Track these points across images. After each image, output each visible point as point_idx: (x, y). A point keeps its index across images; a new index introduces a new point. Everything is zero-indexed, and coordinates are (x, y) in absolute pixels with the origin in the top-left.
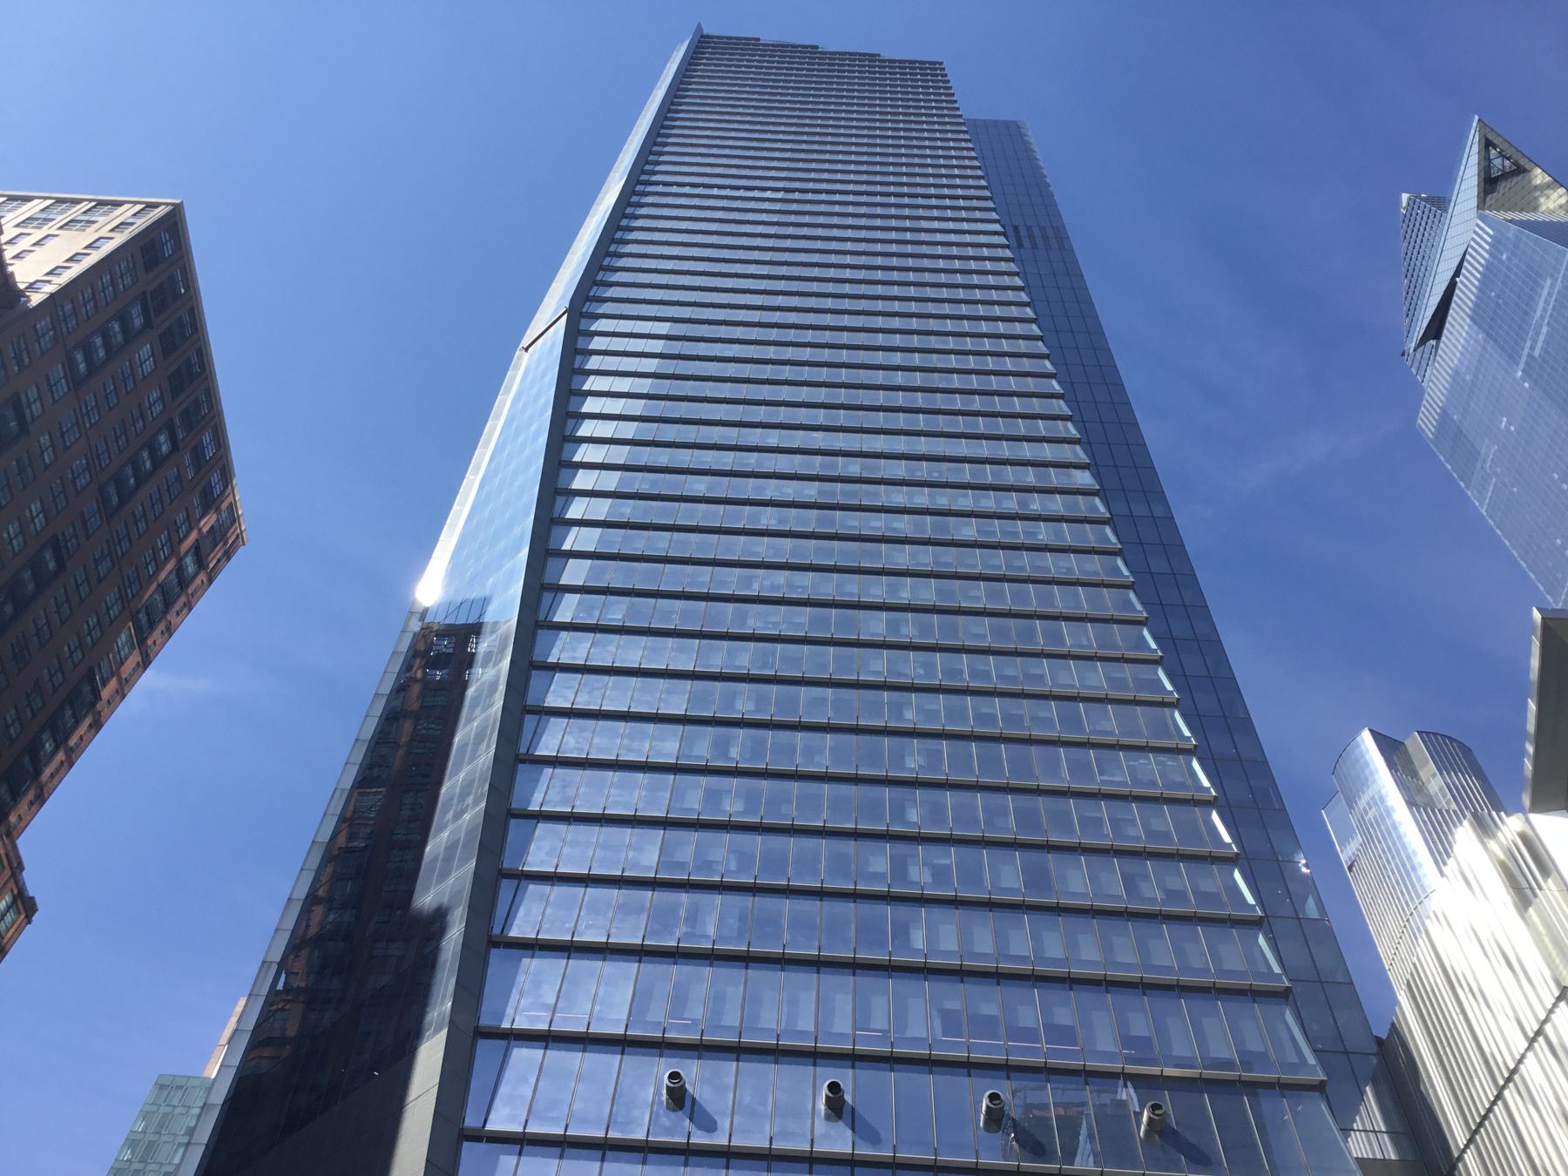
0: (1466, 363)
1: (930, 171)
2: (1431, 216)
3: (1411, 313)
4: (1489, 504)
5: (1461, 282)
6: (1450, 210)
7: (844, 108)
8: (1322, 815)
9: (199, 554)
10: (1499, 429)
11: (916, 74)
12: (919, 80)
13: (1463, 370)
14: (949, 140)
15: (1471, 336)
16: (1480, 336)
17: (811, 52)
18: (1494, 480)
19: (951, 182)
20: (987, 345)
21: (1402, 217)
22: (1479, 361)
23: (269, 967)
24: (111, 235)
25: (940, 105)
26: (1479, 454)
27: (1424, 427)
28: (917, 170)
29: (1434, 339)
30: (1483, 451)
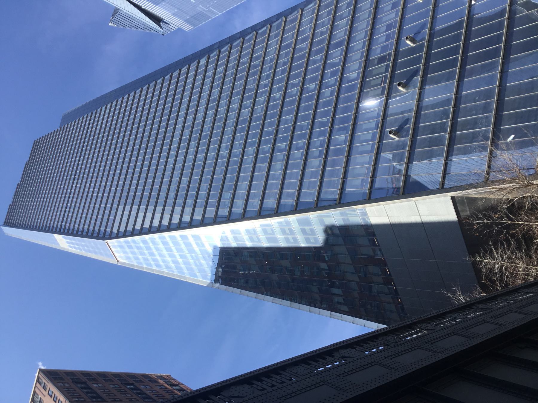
0: (171, 10)
2: (119, 16)
3: (151, 29)
4: (218, 11)
5: (144, 6)
6: (119, 8)
9: (172, 385)
10: (194, 3)
11: (18, 208)
13: (173, 11)
14: (44, 209)
15: (163, 7)
16: (163, 3)
17: (19, 186)
18: (210, 8)
21: (117, 27)
22: (171, 5)
23: (332, 315)
24: (47, 391)
25: (31, 209)
26: (201, 11)
27: (189, 29)
28: (54, 218)
29: (160, 23)
30: (201, 10)
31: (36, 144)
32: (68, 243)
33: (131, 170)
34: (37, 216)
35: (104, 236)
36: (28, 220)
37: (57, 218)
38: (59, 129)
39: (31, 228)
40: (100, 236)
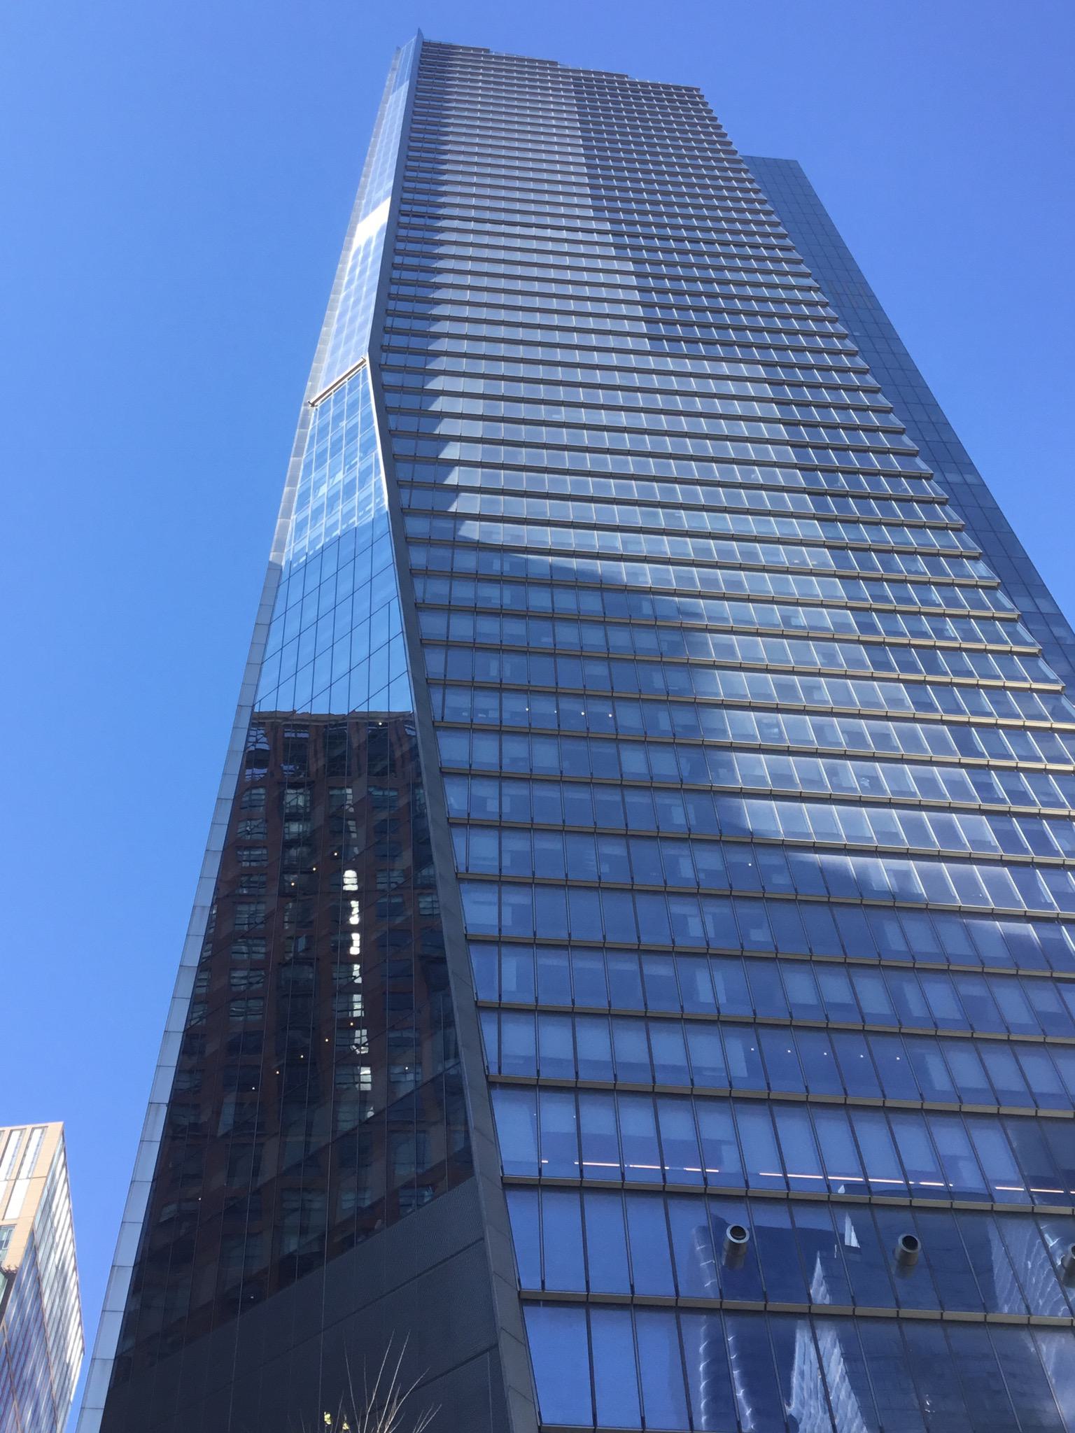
1: (558, 167)
7: (477, 140)
8: (75, 1396)
11: (546, 75)
12: (548, 68)
19: (565, 168)
20: (620, 398)
31: (688, 97)
32: (368, 243)
33: (679, 403)
34: (540, 113)
35: (387, 333)
36: (500, 87)
37: (545, 176)
38: (737, 157)
39: (415, 117)
40: (387, 336)
